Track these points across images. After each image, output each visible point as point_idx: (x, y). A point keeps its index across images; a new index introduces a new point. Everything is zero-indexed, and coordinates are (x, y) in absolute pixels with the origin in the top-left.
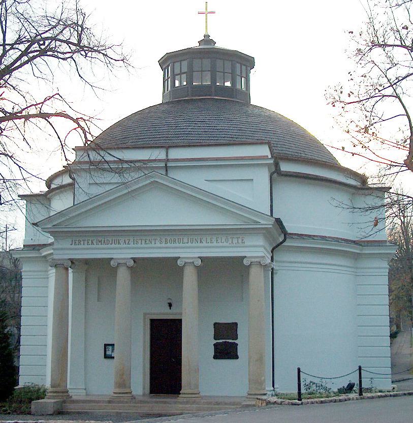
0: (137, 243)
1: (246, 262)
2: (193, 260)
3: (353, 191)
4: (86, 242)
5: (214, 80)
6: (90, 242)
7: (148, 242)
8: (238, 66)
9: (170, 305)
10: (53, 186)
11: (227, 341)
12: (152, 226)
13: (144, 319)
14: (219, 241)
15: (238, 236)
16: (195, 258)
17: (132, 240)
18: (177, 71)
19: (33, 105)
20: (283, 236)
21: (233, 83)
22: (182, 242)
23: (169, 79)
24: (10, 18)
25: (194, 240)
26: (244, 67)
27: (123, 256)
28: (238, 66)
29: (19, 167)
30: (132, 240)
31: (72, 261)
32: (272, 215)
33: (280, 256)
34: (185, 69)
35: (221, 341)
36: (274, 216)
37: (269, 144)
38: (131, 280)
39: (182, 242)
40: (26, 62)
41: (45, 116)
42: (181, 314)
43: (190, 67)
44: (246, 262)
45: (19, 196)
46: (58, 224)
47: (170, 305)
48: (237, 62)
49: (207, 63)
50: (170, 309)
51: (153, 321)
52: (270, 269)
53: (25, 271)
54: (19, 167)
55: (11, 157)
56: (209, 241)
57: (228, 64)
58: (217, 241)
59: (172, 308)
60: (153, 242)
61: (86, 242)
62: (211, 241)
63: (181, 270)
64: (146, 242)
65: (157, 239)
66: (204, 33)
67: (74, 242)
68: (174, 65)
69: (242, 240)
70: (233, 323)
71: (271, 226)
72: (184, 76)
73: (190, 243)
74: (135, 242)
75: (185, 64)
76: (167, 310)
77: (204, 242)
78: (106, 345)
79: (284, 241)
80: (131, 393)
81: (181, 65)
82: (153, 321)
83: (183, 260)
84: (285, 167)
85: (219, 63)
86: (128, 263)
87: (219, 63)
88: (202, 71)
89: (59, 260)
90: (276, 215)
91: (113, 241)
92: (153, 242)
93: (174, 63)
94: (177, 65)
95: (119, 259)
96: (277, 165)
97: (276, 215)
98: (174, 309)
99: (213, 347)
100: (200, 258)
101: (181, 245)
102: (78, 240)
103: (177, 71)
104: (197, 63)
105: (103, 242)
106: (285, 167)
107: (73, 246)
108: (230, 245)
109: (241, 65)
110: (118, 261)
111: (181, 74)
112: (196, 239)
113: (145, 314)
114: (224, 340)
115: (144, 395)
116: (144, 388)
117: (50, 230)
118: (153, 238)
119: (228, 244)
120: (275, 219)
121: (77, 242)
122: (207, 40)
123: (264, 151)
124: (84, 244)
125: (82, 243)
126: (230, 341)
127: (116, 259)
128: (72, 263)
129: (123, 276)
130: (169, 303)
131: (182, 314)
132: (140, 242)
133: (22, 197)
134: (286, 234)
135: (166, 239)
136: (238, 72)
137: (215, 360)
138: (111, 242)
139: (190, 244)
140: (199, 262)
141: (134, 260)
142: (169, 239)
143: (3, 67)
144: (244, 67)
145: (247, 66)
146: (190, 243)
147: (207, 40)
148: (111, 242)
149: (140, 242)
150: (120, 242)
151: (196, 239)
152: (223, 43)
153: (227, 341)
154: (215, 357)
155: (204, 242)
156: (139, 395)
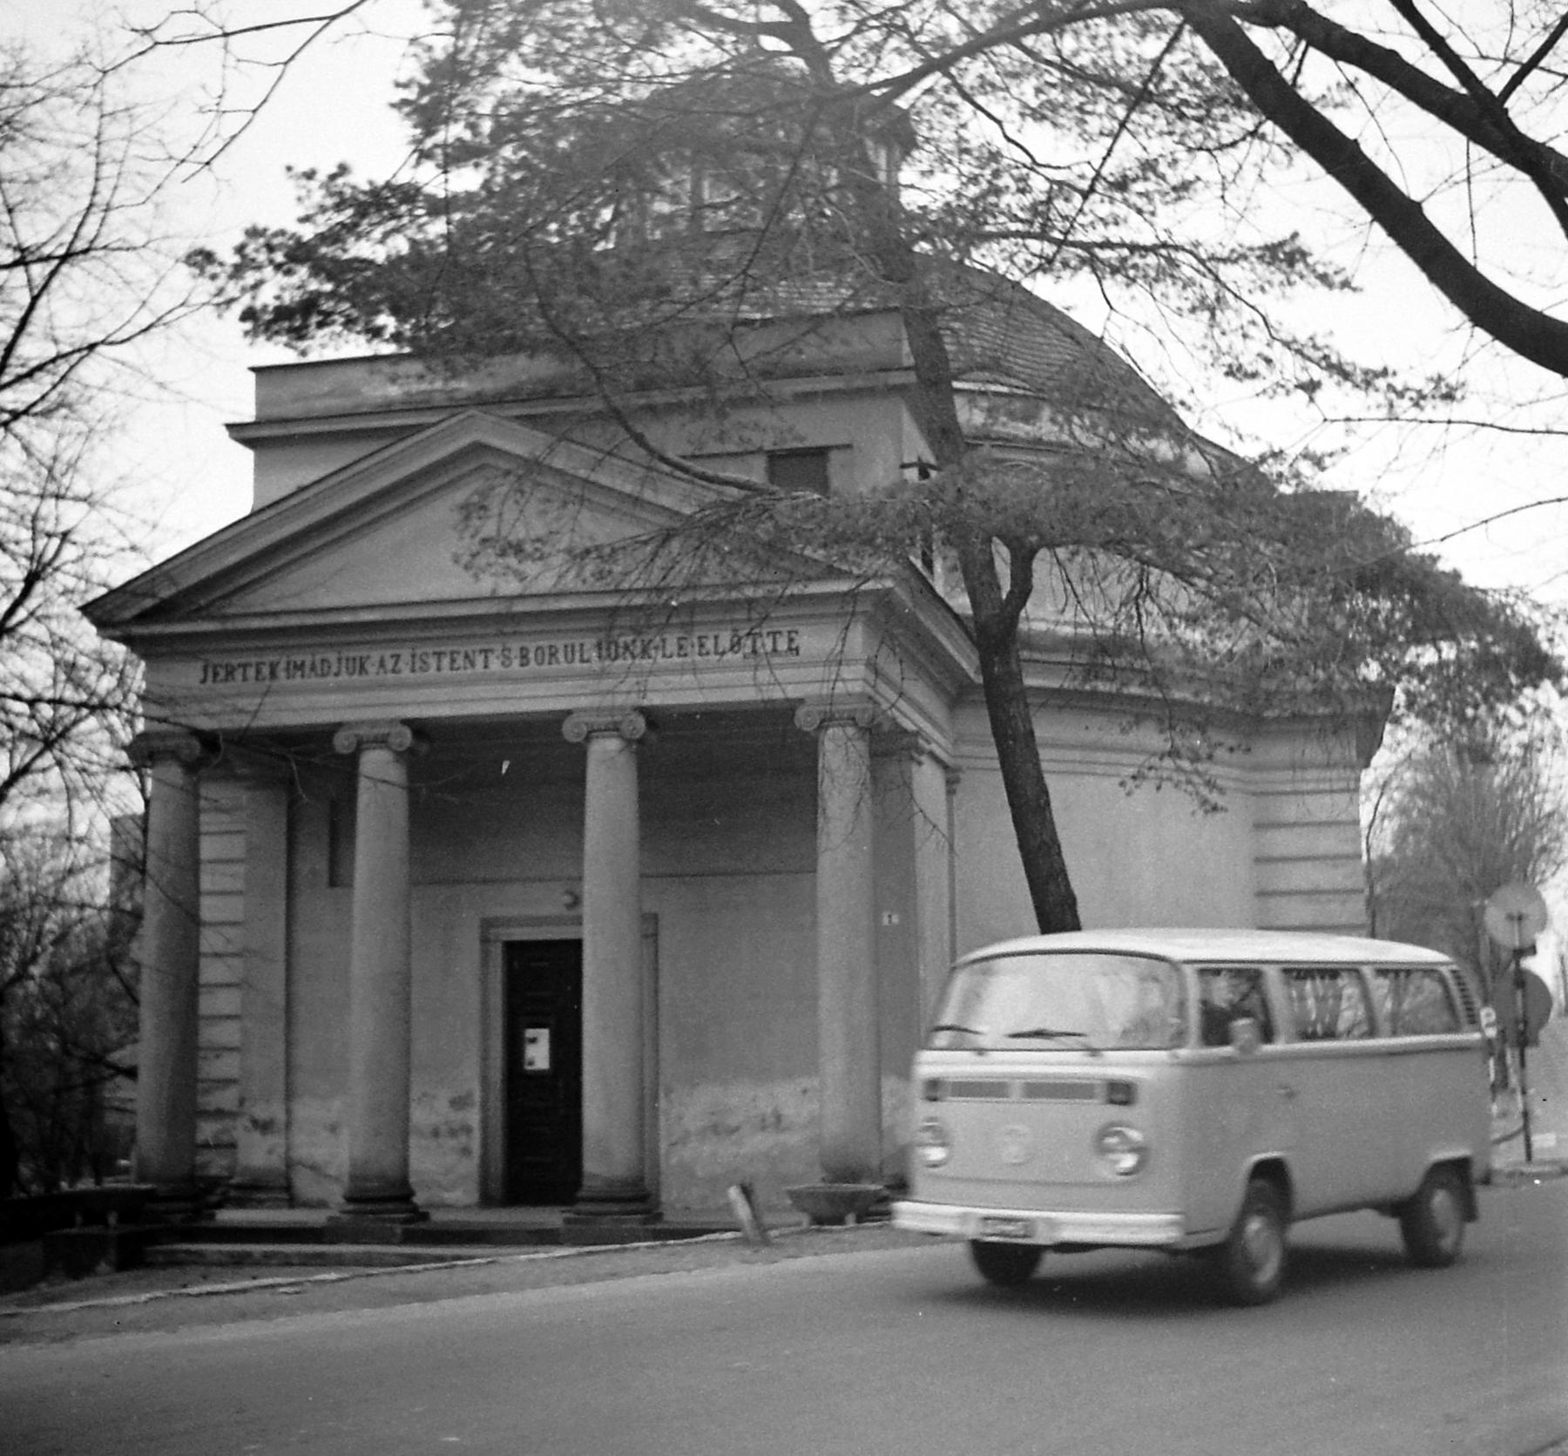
6: (266, 671)
7: (460, 661)
13: (485, 940)
14: (710, 644)
16: (391, 722)
22: (577, 655)
24: (1027, 284)
29: (333, 18)
30: (406, 654)
38: (412, 834)
39: (577, 655)
44: (342, 743)
54: (333, 18)
58: (702, 646)
62: (681, 647)
64: (453, 661)
65: (492, 651)
67: (210, 674)
69: (791, 640)
73: (344, 677)
74: (418, 664)
92: (480, 660)
95: (362, 723)
102: (785, 630)
105: (307, 670)
113: (487, 924)
118: (478, 647)
121: (222, 673)
124: (439, 669)
140: (406, 737)
142: (532, 646)
146: (344, 677)
148: (334, 669)
149: (433, 661)
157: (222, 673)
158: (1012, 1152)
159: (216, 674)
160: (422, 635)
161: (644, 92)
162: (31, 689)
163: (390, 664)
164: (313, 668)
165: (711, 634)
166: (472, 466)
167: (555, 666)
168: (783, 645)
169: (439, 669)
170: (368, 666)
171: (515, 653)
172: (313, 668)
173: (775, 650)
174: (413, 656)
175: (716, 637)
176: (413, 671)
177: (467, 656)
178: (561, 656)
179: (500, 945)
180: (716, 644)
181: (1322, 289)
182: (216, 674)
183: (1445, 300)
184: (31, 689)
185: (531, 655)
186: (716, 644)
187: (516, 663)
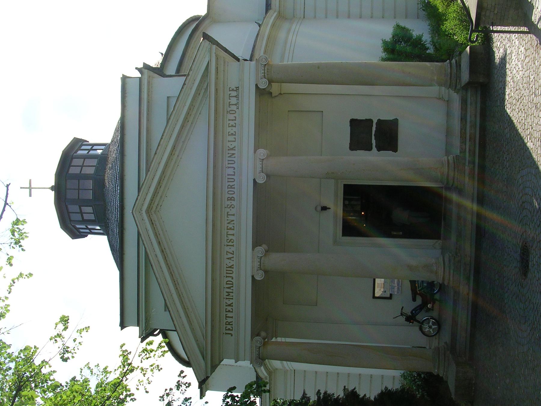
4: (229, 314)
6: (229, 308)
7: (230, 226)
8: (80, 152)
11: (373, 133)
23: (90, 227)
26: (83, 147)
34: (86, 217)
35: (374, 142)
43: (73, 202)
45: (201, 398)
47: (324, 208)
50: (329, 208)
57: (76, 162)
62: (232, 134)
66: (50, 191)
68: (73, 221)
69: (233, 90)
70: (351, 125)
74: (230, 244)
76: (330, 213)
77: (234, 144)
81: (74, 213)
85: (73, 171)
87: (73, 171)
88: (79, 189)
91: (228, 275)
92: (231, 218)
93: (71, 221)
103: (78, 217)
111: (82, 213)
118: (226, 218)
119: (237, 110)
124: (232, 292)
126: (374, 129)
133: (202, 395)
135: (228, 200)
138: (230, 279)
140: (260, 249)
141: (256, 243)
143: (230, 398)
144: (83, 147)
148: (230, 279)
153: (373, 133)
154: (395, 150)
155: (234, 144)
157: (229, 327)
158: (353, 202)
159: (229, 329)
160: (225, 152)
161: (120, 121)
162: (228, 304)
163: (230, 256)
166: (201, 108)
167: (235, 186)
168: (234, 94)
169: (233, 235)
170: (232, 132)
171: (229, 203)
173: (235, 96)
174: (227, 298)
175: (229, 120)
176: (233, 246)
178: (231, 184)
179: (342, 237)
180: (232, 120)
181: (164, 180)
182: (229, 329)
183: (119, 297)
184: (228, 304)
185: (231, 196)
186: (232, 120)
187: (233, 202)
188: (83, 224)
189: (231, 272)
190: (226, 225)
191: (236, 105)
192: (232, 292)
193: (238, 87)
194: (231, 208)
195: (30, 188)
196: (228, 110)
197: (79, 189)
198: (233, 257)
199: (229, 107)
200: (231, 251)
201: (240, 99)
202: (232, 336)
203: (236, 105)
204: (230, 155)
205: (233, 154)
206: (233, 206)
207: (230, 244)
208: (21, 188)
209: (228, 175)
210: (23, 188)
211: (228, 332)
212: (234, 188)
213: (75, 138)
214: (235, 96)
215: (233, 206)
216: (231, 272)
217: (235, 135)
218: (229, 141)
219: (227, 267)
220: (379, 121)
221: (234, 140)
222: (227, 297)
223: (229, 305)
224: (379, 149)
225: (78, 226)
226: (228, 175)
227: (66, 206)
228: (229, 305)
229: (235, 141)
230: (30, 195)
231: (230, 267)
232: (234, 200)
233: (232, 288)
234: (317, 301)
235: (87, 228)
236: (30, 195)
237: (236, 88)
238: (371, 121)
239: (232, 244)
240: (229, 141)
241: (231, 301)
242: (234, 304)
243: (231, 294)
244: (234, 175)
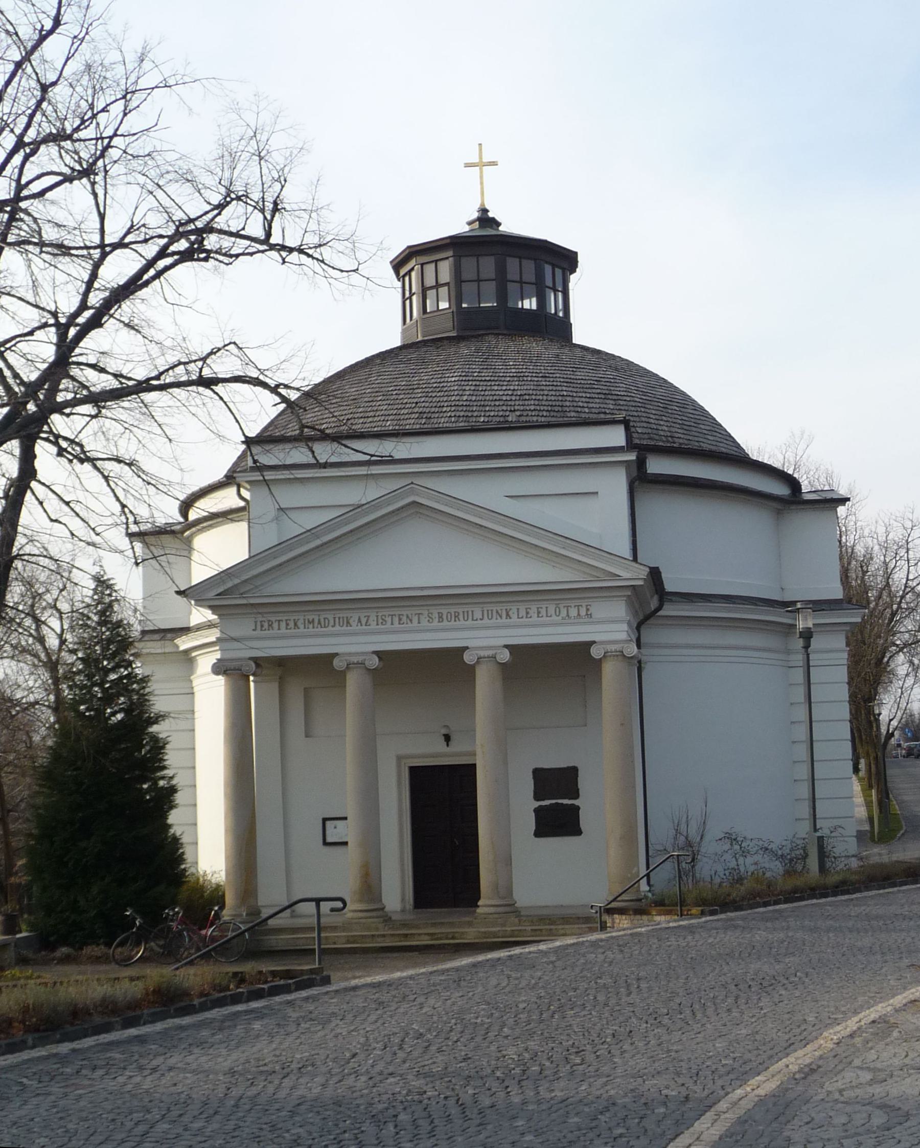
0: (384, 622)
1: (338, 664)
2: (364, 657)
3: (775, 505)
4: (283, 625)
5: (502, 296)
6: (292, 624)
7: (404, 619)
8: (548, 269)
9: (447, 738)
10: (193, 515)
11: (560, 801)
12: (422, 588)
13: (399, 766)
14: (543, 612)
15: (578, 602)
17: (373, 617)
18: (430, 281)
19: (180, 363)
20: (656, 598)
21: (542, 302)
22: (470, 617)
23: (414, 298)
25: (494, 613)
26: (558, 272)
27: (353, 649)
28: (548, 269)
30: (373, 617)
31: (257, 661)
32: (635, 559)
33: (649, 635)
36: (639, 561)
37: (626, 423)
39: (470, 617)
40: (154, 278)
41: (208, 383)
42: (474, 754)
46: (225, 591)
48: (547, 263)
49: (488, 265)
50: (448, 745)
51: (415, 772)
52: (636, 662)
53: (842, 651)
55: (130, 465)
56: (551, 610)
57: (529, 267)
58: (539, 613)
59: (450, 743)
60: (415, 620)
61: (283, 625)
62: (527, 613)
63: (470, 671)
65: (282, 620)
66: (477, 206)
69: (588, 610)
71: (641, 583)
72: (444, 291)
74: (380, 621)
75: (446, 271)
76: (441, 747)
77: (514, 616)
78: (325, 820)
79: (659, 608)
80: (383, 909)
82: (415, 772)
83: (474, 652)
84: (657, 466)
85: (512, 265)
86: (367, 663)
89: (357, 654)
90: (649, 557)
92: (415, 620)
94: (430, 269)
95: (350, 654)
96: (641, 463)
97: (649, 557)
98: (457, 746)
99: (534, 814)
100: (506, 646)
101: (470, 622)
104: (469, 264)
105: (316, 624)
106: (657, 466)
107: (259, 633)
108: (564, 621)
109: (554, 266)
110: (348, 658)
111: (438, 286)
112: (497, 612)
113: (399, 758)
114: (554, 801)
115: (403, 911)
116: (403, 900)
117: (212, 603)
119: (560, 618)
120: (650, 568)
122: (485, 220)
123: (615, 436)
125: (275, 625)
127: (602, 643)
128: (258, 665)
129: (354, 683)
130: (444, 735)
131: (475, 755)
132: (389, 619)
134: (663, 596)
136: (549, 282)
137: (537, 839)
139: (486, 621)
140: (374, 662)
145: (564, 270)
147: (485, 220)
150: (351, 621)
151: (497, 612)
152: (512, 225)
153: (560, 801)
154: (538, 833)
155: (514, 616)
156: (396, 912)
163: (364, 621)
164: (319, 623)
165: (544, 606)
167: (458, 623)
168: (583, 612)
172: (319, 623)
173: (579, 615)
174: (304, 620)
176: (377, 624)
177: (408, 617)
178: (461, 617)
182: (262, 626)
185: (444, 617)
188: (417, 288)
189: (341, 624)
190: (404, 613)
191: (568, 615)
192: (313, 628)
193: (591, 617)
194: (428, 618)
195: (481, 165)
196: (560, 606)
197: (479, 280)
198: (361, 625)
199: (564, 607)
200: (370, 621)
201: (576, 621)
202: (254, 630)
203: (568, 615)
204: (500, 612)
205: (501, 617)
206: (431, 620)
207: (380, 621)
208: (480, 144)
209: (472, 611)
210: (480, 150)
211: (259, 624)
212: (455, 621)
213: (576, 253)
214: (579, 615)
215: (431, 620)
216: (341, 624)
217: (527, 617)
218: (518, 609)
219: (347, 618)
220: (578, 808)
221: (520, 616)
222: (307, 622)
223: (296, 624)
224: (537, 811)
225: (413, 274)
226: (472, 611)
227: (447, 258)
228: (296, 624)
229: (518, 618)
230: (468, 165)
231: (348, 622)
232: (439, 622)
233: (319, 626)
234: (272, 493)
235: (411, 294)
236: (468, 165)
237: (591, 614)
238: (577, 796)
239: (380, 623)
240: (518, 609)
241: (302, 626)
242: (297, 630)
243: (311, 626)
244: (473, 620)
